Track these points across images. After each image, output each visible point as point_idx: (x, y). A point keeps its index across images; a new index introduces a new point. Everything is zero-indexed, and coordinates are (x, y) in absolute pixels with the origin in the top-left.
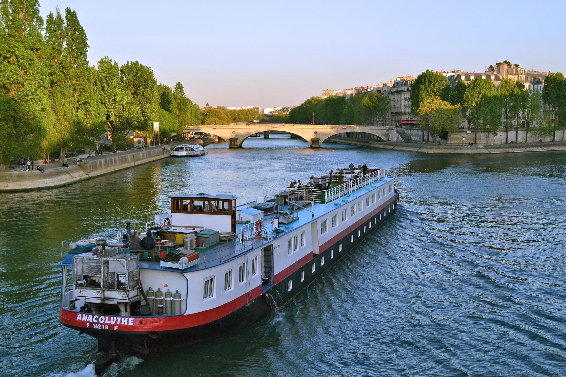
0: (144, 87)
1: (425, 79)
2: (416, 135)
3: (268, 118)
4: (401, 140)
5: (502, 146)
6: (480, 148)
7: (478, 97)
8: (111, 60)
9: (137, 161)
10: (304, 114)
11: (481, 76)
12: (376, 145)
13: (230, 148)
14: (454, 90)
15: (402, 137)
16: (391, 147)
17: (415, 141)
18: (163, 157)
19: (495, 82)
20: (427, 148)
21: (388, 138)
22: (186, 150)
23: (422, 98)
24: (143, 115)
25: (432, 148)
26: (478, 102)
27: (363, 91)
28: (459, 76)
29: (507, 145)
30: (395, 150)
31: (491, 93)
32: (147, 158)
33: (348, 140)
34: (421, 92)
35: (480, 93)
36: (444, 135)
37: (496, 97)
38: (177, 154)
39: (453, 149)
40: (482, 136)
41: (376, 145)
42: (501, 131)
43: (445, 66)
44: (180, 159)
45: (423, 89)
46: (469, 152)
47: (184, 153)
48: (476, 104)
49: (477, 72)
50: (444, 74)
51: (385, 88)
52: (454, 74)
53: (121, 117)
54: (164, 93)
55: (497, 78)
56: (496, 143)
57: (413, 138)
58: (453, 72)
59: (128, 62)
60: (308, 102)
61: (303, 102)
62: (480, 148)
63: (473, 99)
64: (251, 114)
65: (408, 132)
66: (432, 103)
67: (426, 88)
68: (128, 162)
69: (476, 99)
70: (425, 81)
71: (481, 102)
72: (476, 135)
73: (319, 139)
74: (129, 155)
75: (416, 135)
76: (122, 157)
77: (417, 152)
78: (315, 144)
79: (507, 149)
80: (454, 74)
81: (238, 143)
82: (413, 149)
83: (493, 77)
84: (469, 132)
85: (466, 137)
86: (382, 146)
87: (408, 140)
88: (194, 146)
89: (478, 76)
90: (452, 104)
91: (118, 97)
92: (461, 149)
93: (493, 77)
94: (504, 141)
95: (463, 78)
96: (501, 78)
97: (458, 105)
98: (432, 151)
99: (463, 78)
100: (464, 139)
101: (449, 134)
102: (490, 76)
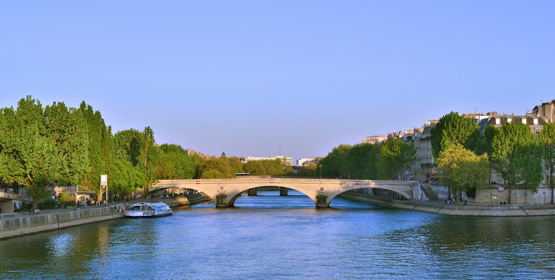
0: (71, 132)
1: (449, 122)
2: (443, 193)
3: (296, 171)
4: (425, 198)
5: (545, 206)
6: (513, 209)
7: (510, 145)
8: (34, 101)
9: (63, 222)
10: (328, 168)
11: (521, 119)
12: (397, 204)
13: (217, 207)
14: (482, 136)
15: (426, 194)
16: (411, 207)
17: (442, 200)
18: (110, 217)
19: (539, 126)
20: (448, 209)
21: (413, 196)
22: (143, 209)
23: (445, 146)
24: (69, 167)
25: (453, 209)
26: (510, 152)
27: (395, 138)
28: (493, 119)
29: (552, 206)
30: (416, 211)
31: (524, 142)
32: (81, 218)
33: (374, 198)
34: (444, 139)
35: (512, 140)
36: (472, 193)
37: (533, 146)
38: (131, 214)
39: (479, 210)
40: (518, 195)
41: (397, 204)
42: (544, 188)
43: (475, 107)
44: (135, 220)
45: (446, 135)
46: (499, 213)
47: (140, 214)
48: (508, 153)
49: (516, 114)
50: (477, 117)
51: (416, 134)
52: (487, 117)
53: (40, 168)
54: (134, 140)
55: (541, 122)
56: (537, 202)
57: (440, 196)
58: (488, 114)
59: (55, 103)
60: (335, 151)
61: (331, 151)
62: (513, 209)
63: (503, 150)
64: (275, 166)
65: (434, 188)
66: (455, 153)
67: (449, 134)
68: (48, 224)
69: (508, 147)
70: (447, 125)
71: (513, 152)
72: (510, 192)
73: (326, 197)
74: (49, 216)
75: (443, 193)
76: (37, 218)
77: (437, 213)
78: (322, 202)
79: (551, 211)
80: (487, 117)
81: (227, 201)
82: (433, 210)
83: (536, 121)
84: (501, 189)
85: (498, 195)
86: (402, 206)
87: (433, 197)
88: (154, 204)
89: (517, 120)
90: (479, 153)
91: (37, 144)
92: (489, 210)
93: (536, 121)
94: (549, 200)
95: (498, 121)
96: (547, 121)
97: (485, 155)
98: (454, 213)
99: (498, 121)
100: (495, 198)
101: (477, 191)
102: (532, 119)
